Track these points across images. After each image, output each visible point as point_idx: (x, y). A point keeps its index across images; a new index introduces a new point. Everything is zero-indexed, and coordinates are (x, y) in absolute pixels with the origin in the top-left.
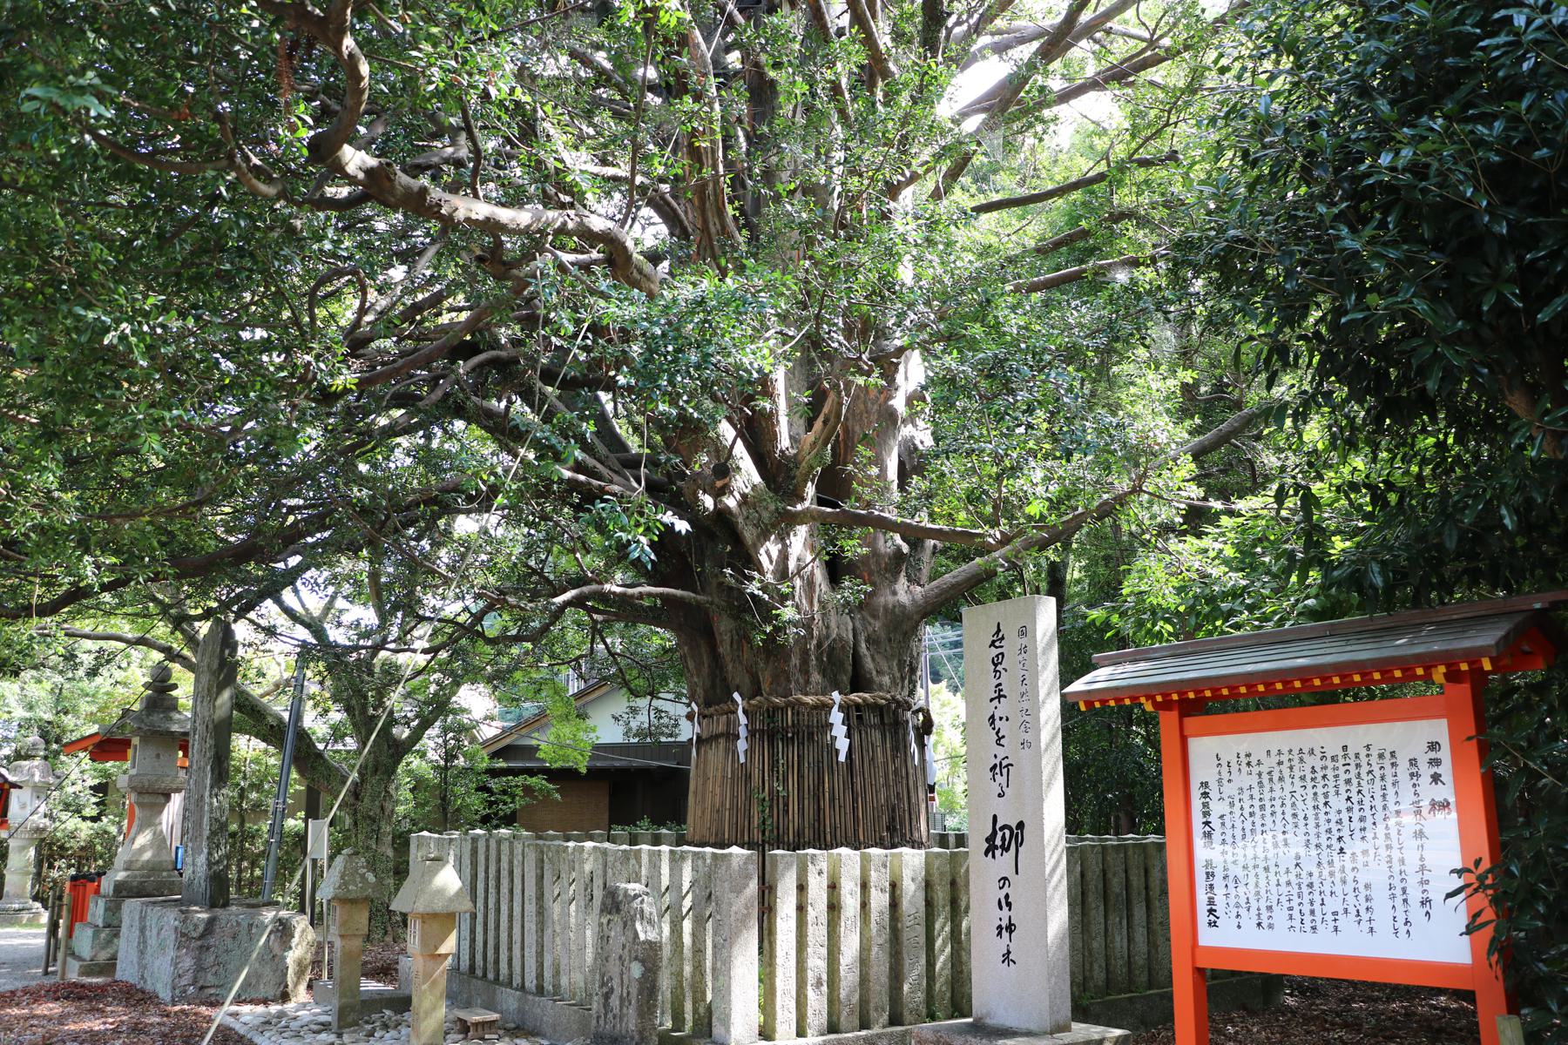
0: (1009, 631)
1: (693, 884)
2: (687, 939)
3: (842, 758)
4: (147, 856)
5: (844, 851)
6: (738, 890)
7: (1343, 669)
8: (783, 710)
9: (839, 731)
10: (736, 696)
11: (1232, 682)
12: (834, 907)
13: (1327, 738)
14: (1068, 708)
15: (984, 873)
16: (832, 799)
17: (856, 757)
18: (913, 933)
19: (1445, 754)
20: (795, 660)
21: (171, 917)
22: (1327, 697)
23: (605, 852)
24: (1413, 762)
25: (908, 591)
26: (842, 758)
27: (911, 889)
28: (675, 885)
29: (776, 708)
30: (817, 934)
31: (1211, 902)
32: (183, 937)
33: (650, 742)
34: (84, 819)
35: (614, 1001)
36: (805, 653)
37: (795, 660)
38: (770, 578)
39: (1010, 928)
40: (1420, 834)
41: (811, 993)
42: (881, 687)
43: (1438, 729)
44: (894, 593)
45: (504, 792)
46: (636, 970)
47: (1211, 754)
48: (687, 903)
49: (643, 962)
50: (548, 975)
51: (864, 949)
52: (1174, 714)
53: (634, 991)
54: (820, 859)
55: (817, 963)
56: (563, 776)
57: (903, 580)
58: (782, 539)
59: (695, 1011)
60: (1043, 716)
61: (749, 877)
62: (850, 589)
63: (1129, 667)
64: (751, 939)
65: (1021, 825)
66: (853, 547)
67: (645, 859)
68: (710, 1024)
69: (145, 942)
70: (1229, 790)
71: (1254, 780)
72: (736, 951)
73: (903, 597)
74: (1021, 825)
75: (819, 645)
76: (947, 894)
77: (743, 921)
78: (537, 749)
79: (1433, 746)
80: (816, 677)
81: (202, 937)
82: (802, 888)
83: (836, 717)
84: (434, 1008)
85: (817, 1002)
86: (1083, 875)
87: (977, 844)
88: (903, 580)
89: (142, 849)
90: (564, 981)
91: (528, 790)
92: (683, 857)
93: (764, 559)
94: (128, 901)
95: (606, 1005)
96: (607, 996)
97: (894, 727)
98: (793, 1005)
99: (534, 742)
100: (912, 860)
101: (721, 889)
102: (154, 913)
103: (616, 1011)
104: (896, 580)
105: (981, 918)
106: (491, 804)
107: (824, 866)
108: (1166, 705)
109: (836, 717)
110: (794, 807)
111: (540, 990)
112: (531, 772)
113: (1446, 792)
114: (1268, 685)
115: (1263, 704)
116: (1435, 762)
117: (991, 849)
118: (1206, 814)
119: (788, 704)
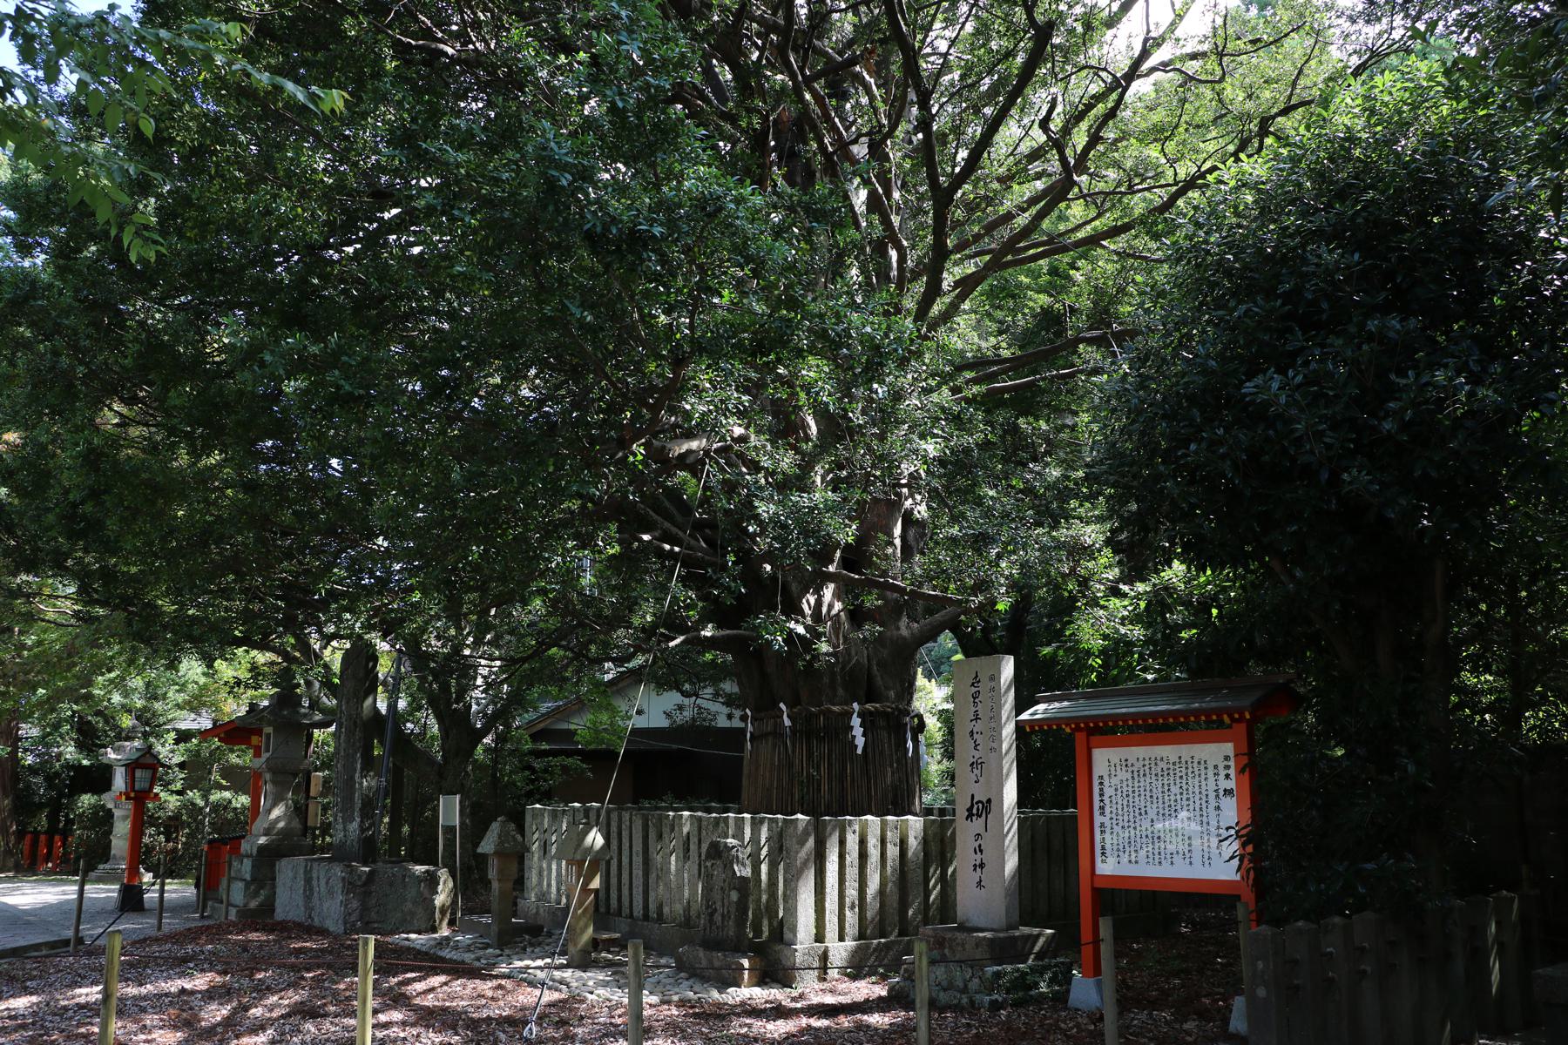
0: (983, 677)
1: (768, 839)
2: (764, 877)
3: (859, 751)
4: (281, 825)
5: (869, 817)
6: (802, 843)
7: (1175, 714)
8: (817, 716)
9: (858, 731)
10: (782, 705)
11: (1115, 718)
12: (863, 856)
13: (1168, 752)
14: (1020, 727)
15: (966, 832)
16: (853, 781)
17: (869, 749)
18: (915, 876)
19: (1232, 763)
20: (826, 680)
21: (338, 871)
22: (1166, 728)
23: (700, 819)
24: (1216, 767)
25: (908, 627)
26: (859, 751)
27: (913, 843)
28: (755, 839)
29: (812, 714)
30: (852, 873)
31: (1103, 848)
32: (349, 886)
33: (696, 732)
34: (172, 792)
35: (718, 918)
36: (833, 674)
37: (826, 680)
38: (809, 621)
39: (982, 866)
40: (1218, 808)
41: (848, 913)
42: (887, 699)
43: (1228, 748)
44: (898, 628)
45: (546, 771)
46: (734, 896)
47: (1105, 760)
48: (764, 852)
49: (739, 890)
50: (652, 906)
51: (883, 884)
52: (1084, 735)
53: (733, 910)
54: (855, 823)
55: (852, 893)
56: (600, 758)
57: (905, 620)
58: (818, 592)
59: (770, 924)
60: (1004, 733)
61: (808, 835)
62: (870, 629)
63: (1057, 705)
64: (810, 876)
65: (989, 801)
66: (872, 601)
67: (731, 823)
68: (782, 933)
69: (311, 889)
70: (1115, 781)
71: (1129, 775)
72: (801, 883)
73: (904, 632)
74: (989, 801)
75: (843, 668)
76: (939, 845)
77: (805, 863)
78: (574, 733)
79: (1227, 758)
80: (840, 691)
81: (365, 884)
82: (842, 843)
83: (856, 721)
84: (586, 927)
85: (851, 918)
86: (1033, 837)
87: (961, 812)
88: (905, 620)
89: (278, 820)
90: (666, 910)
91: (565, 769)
92: (762, 821)
93: (805, 606)
94: (284, 861)
95: (711, 921)
96: (712, 915)
97: (897, 724)
98: (836, 920)
99: (573, 727)
100: (915, 823)
101: (790, 843)
102: (319, 872)
103: (719, 923)
104: (899, 619)
105: (962, 865)
106: (532, 781)
107: (857, 827)
108: (1078, 729)
109: (856, 721)
110: (825, 787)
111: (646, 917)
112: (569, 754)
113: (1231, 784)
114: (1135, 721)
115: (1132, 730)
116: (1227, 767)
117: (970, 816)
118: (1101, 795)
119: (821, 712)
